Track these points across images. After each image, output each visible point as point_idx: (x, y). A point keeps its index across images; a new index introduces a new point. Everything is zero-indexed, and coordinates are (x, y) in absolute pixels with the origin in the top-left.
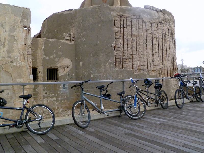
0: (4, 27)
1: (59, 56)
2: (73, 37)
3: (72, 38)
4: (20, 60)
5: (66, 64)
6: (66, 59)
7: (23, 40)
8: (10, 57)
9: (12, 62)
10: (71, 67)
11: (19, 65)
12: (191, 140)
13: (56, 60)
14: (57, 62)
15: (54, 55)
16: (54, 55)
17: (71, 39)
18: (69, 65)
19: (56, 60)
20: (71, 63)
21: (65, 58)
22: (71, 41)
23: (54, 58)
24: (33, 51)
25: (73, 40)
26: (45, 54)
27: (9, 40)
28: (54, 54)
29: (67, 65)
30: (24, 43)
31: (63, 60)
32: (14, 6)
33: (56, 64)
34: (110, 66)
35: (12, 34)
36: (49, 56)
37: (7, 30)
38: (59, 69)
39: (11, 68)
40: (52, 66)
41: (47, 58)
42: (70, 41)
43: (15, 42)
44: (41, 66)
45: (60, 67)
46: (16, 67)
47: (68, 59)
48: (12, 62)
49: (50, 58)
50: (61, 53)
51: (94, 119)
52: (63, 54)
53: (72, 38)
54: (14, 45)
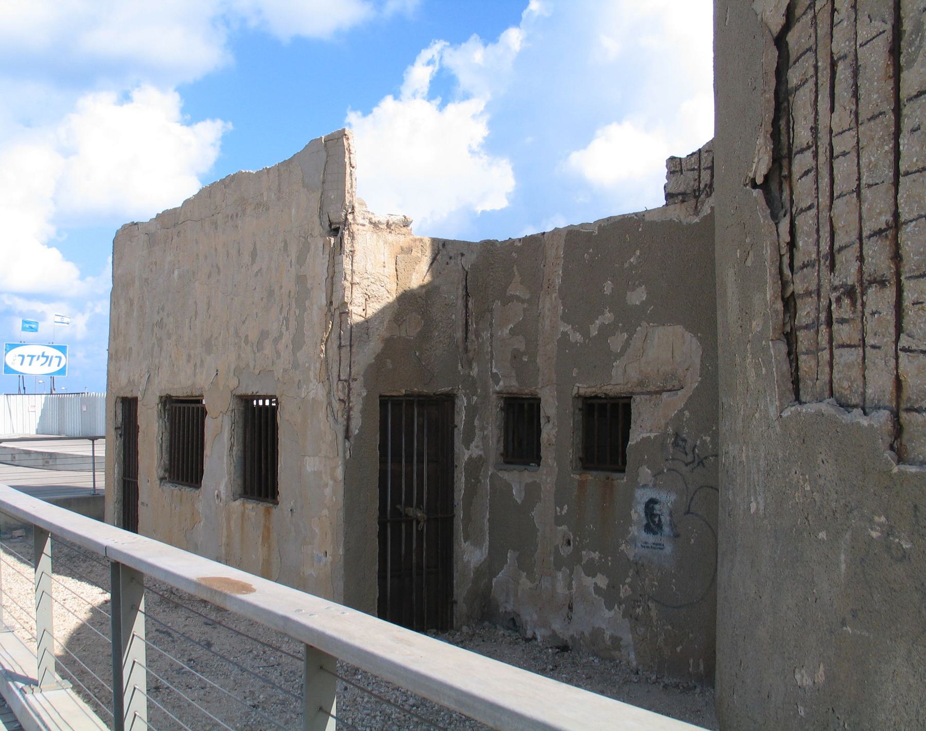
1: (629, 319)
11: (311, 395)
15: (608, 317)
17: (702, 186)
22: (702, 196)
23: (606, 331)
26: (565, 318)
41: (577, 337)
47: (679, 329)
49: (586, 334)
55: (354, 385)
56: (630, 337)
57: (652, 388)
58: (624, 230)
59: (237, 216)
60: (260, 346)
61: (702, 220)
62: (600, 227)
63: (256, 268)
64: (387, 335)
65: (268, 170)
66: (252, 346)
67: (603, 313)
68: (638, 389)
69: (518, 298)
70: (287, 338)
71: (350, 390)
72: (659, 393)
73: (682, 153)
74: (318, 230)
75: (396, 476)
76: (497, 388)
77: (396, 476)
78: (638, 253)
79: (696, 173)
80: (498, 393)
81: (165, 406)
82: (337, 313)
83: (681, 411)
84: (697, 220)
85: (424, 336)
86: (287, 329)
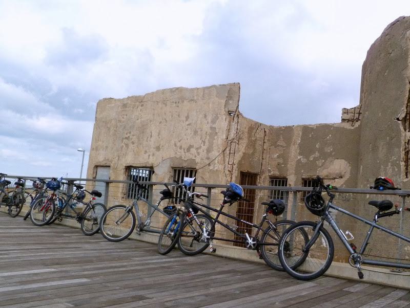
0: (207, 117)
1: (325, 156)
2: (360, 113)
3: (357, 116)
4: (218, 162)
5: (337, 172)
6: (339, 160)
7: (225, 132)
8: (208, 158)
9: (209, 165)
10: (347, 176)
11: (216, 168)
12: (59, 275)
13: (319, 163)
14: (320, 167)
15: (317, 154)
16: (317, 154)
17: (355, 118)
18: (343, 173)
19: (319, 163)
20: (349, 169)
21: (338, 159)
22: (355, 121)
23: (316, 159)
24: (284, 150)
25: (358, 120)
26: (300, 154)
27: (211, 135)
28: (317, 152)
29: (340, 173)
30: (224, 137)
31: (333, 163)
32: (220, 85)
33: (318, 172)
34: (393, 171)
35: (214, 126)
36: (307, 157)
37: (210, 121)
38: (326, 180)
39: (207, 173)
40: (312, 175)
41: (304, 160)
42: (353, 122)
43: (216, 137)
44: (293, 175)
45: (327, 176)
46: (212, 171)
47: (343, 160)
48: (209, 165)
49: (308, 160)
50: (329, 149)
51: (152, 242)
52: (332, 152)
53: (357, 116)
54: (214, 141)
55: (235, 167)
56: (325, 161)
57: (331, 177)
58: (326, 128)
59: (179, 103)
60: (188, 150)
61: (354, 129)
62: (317, 127)
63: (187, 123)
64: (244, 151)
65: (198, 89)
66: (184, 149)
67: (315, 153)
68: (326, 178)
69: (281, 146)
70: (204, 148)
71: (233, 168)
72: (334, 179)
73: (349, 108)
74: (223, 112)
75: (4, 223)
76: (270, 174)
77: (4, 223)
78: (330, 135)
79: (353, 114)
80: (269, 176)
81: (126, 170)
82: (230, 142)
83: (342, 185)
84: (353, 128)
85: (253, 154)
86: (204, 145)
